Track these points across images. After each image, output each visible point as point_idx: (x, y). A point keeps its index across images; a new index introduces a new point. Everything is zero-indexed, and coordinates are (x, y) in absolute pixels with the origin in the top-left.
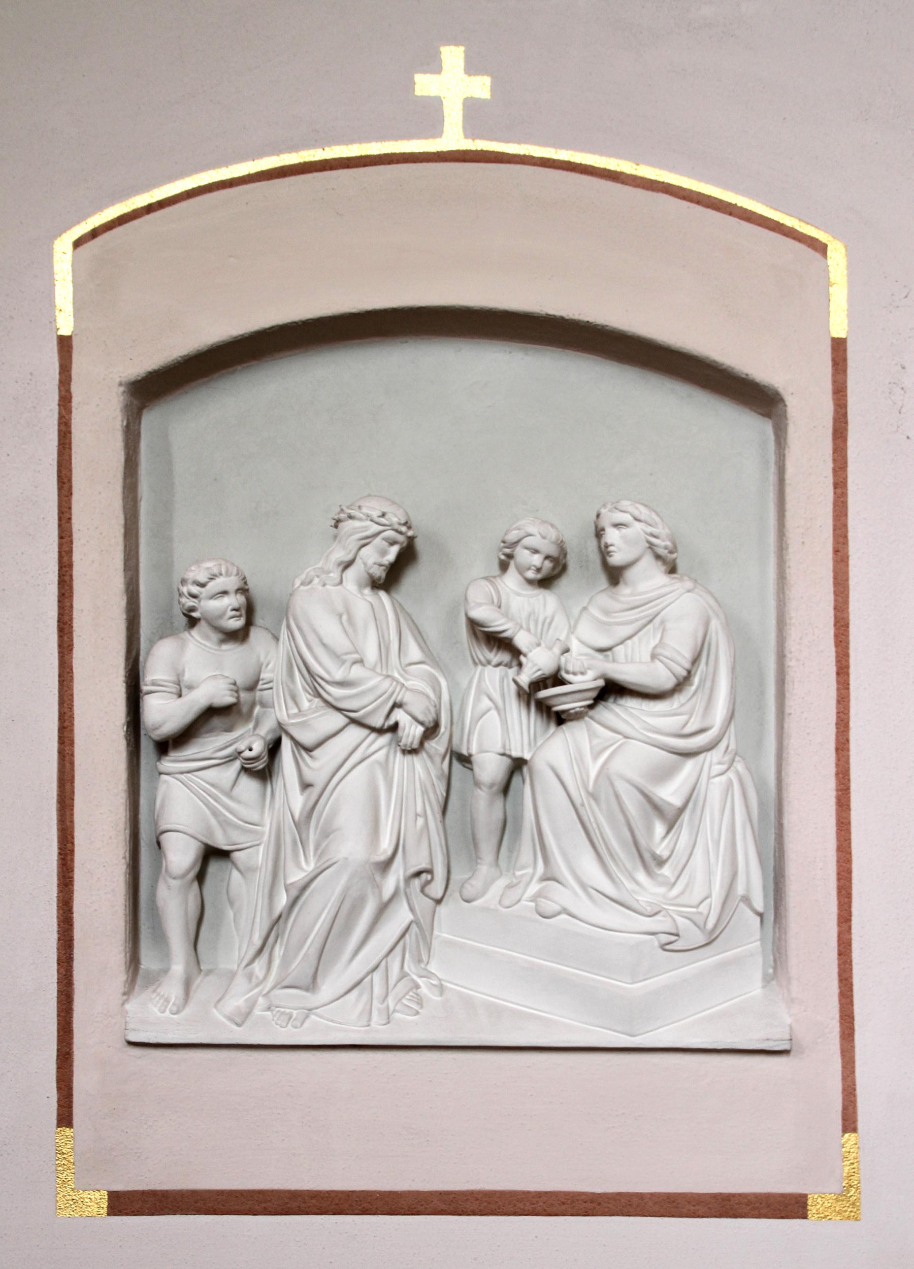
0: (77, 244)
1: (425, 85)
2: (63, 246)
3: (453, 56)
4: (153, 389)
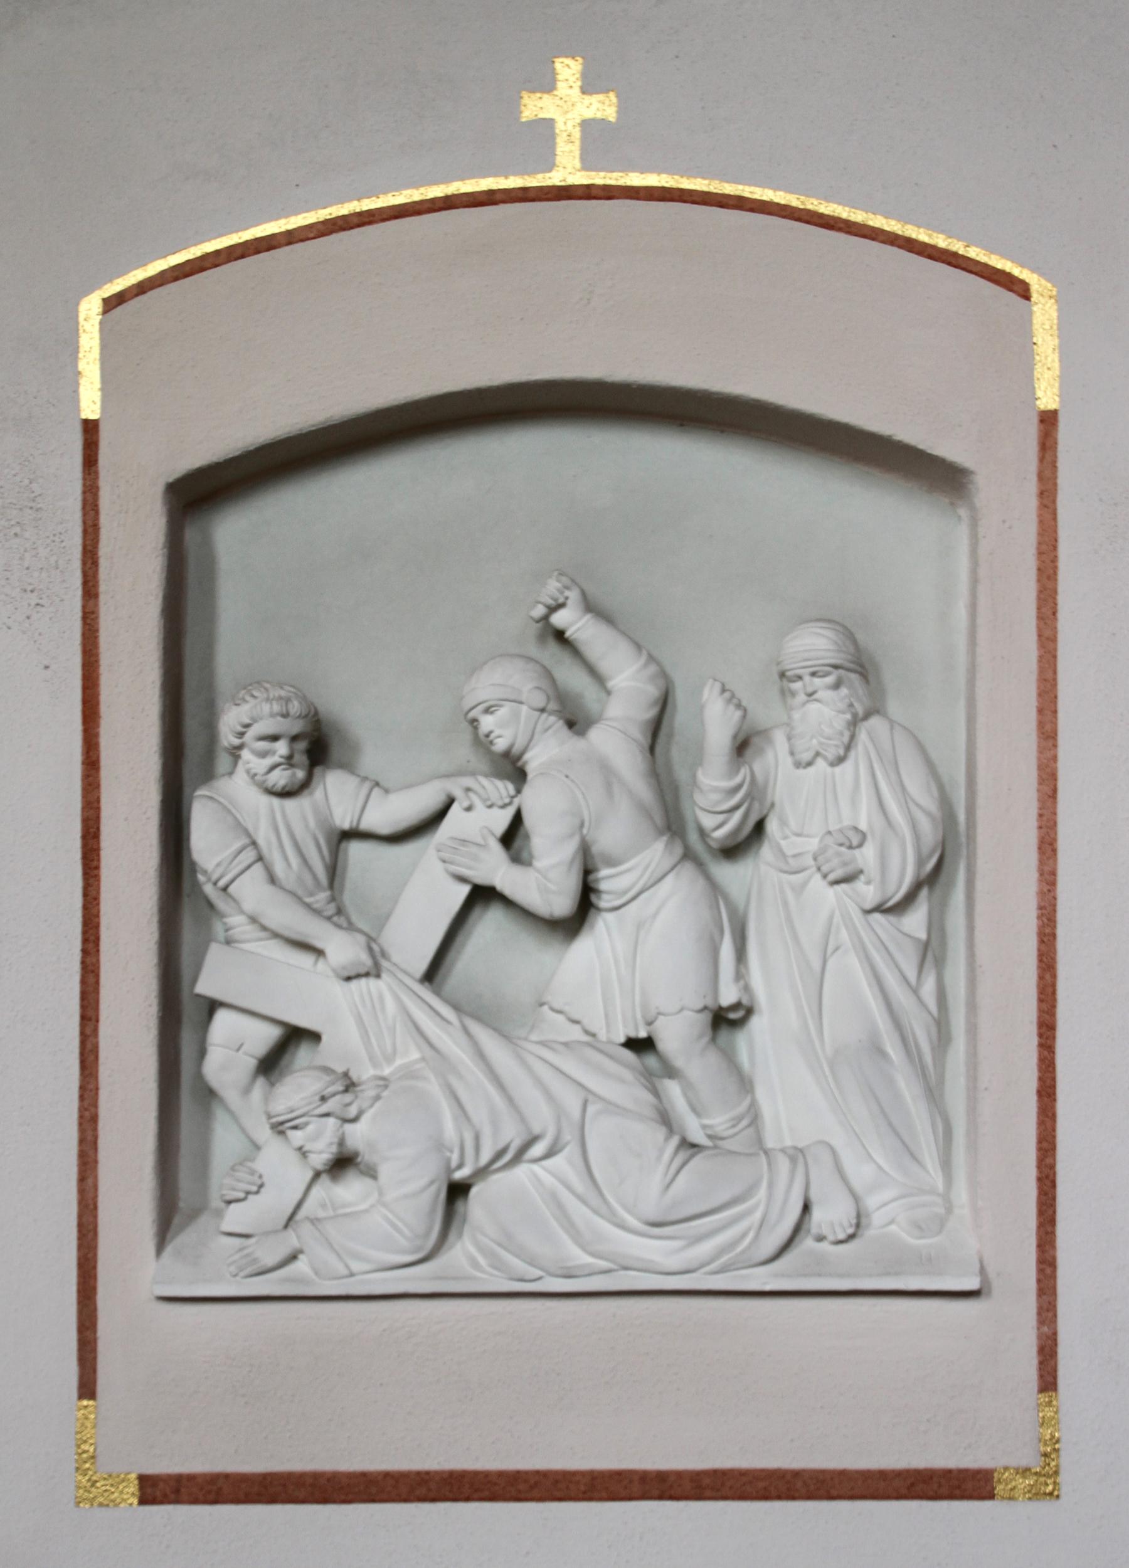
0: (111, 304)
1: (534, 107)
3: (568, 70)
4: (199, 495)
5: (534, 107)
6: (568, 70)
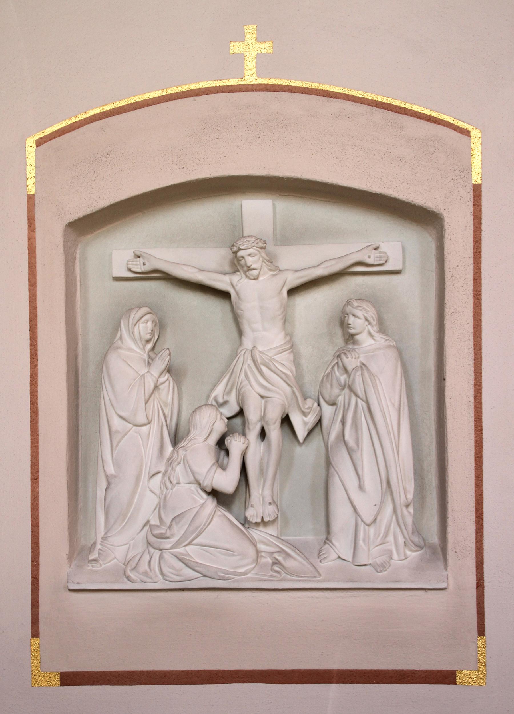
1: (236, 48)
2: (31, 142)
3: (250, 30)
5: (236, 48)
6: (250, 30)
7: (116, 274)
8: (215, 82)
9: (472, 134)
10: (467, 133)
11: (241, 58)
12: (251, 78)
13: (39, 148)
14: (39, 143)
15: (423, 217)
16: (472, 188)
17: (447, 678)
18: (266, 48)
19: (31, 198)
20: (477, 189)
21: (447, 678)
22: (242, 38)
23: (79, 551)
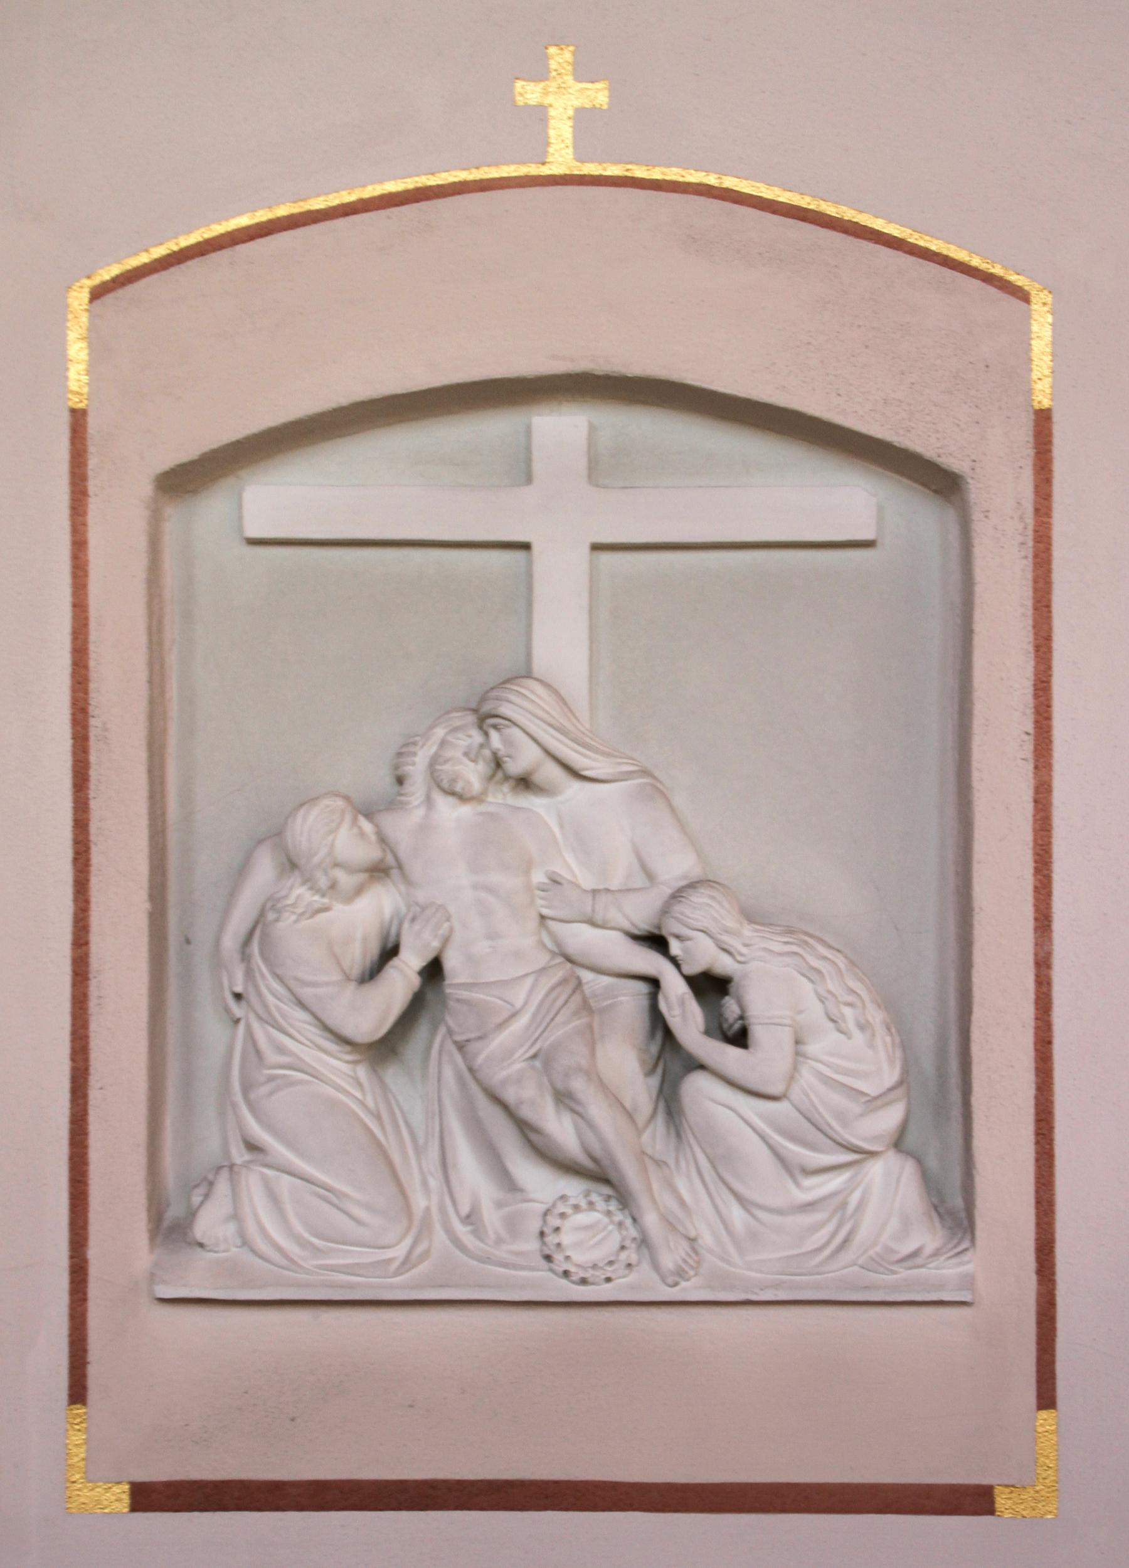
2: (79, 298)
5: (529, 93)
6: (560, 58)
7: (253, 532)
8: (853, 212)
9: (1033, 299)
10: (1023, 296)
11: (540, 114)
12: (561, 159)
13: (98, 302)
14: (98, 293)
15: (940, 482)
16: (1032, 417)
17: (976, 1500)
18: (598, 95)
19: (78, 418)
20: (1043, 419)
21: (976, 1500)
22: (540, 74)
23: (171, 1229)
